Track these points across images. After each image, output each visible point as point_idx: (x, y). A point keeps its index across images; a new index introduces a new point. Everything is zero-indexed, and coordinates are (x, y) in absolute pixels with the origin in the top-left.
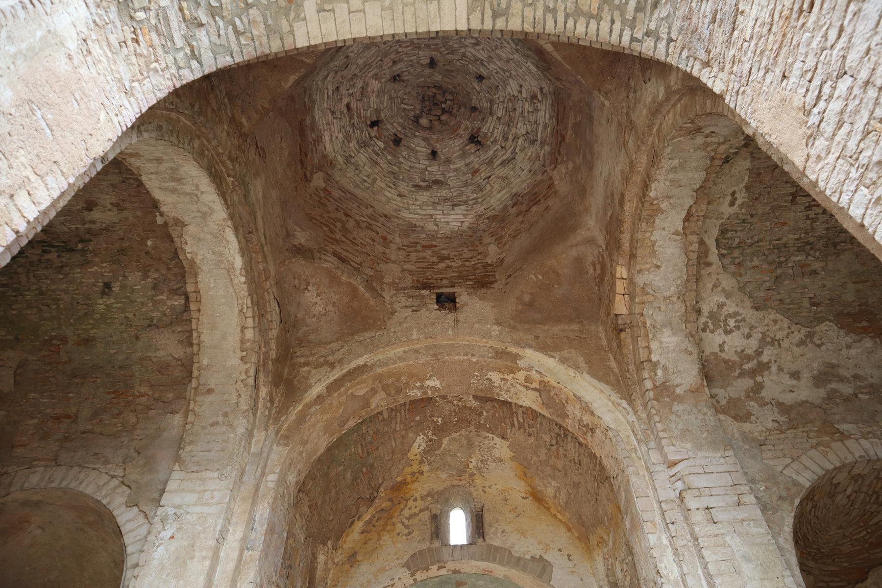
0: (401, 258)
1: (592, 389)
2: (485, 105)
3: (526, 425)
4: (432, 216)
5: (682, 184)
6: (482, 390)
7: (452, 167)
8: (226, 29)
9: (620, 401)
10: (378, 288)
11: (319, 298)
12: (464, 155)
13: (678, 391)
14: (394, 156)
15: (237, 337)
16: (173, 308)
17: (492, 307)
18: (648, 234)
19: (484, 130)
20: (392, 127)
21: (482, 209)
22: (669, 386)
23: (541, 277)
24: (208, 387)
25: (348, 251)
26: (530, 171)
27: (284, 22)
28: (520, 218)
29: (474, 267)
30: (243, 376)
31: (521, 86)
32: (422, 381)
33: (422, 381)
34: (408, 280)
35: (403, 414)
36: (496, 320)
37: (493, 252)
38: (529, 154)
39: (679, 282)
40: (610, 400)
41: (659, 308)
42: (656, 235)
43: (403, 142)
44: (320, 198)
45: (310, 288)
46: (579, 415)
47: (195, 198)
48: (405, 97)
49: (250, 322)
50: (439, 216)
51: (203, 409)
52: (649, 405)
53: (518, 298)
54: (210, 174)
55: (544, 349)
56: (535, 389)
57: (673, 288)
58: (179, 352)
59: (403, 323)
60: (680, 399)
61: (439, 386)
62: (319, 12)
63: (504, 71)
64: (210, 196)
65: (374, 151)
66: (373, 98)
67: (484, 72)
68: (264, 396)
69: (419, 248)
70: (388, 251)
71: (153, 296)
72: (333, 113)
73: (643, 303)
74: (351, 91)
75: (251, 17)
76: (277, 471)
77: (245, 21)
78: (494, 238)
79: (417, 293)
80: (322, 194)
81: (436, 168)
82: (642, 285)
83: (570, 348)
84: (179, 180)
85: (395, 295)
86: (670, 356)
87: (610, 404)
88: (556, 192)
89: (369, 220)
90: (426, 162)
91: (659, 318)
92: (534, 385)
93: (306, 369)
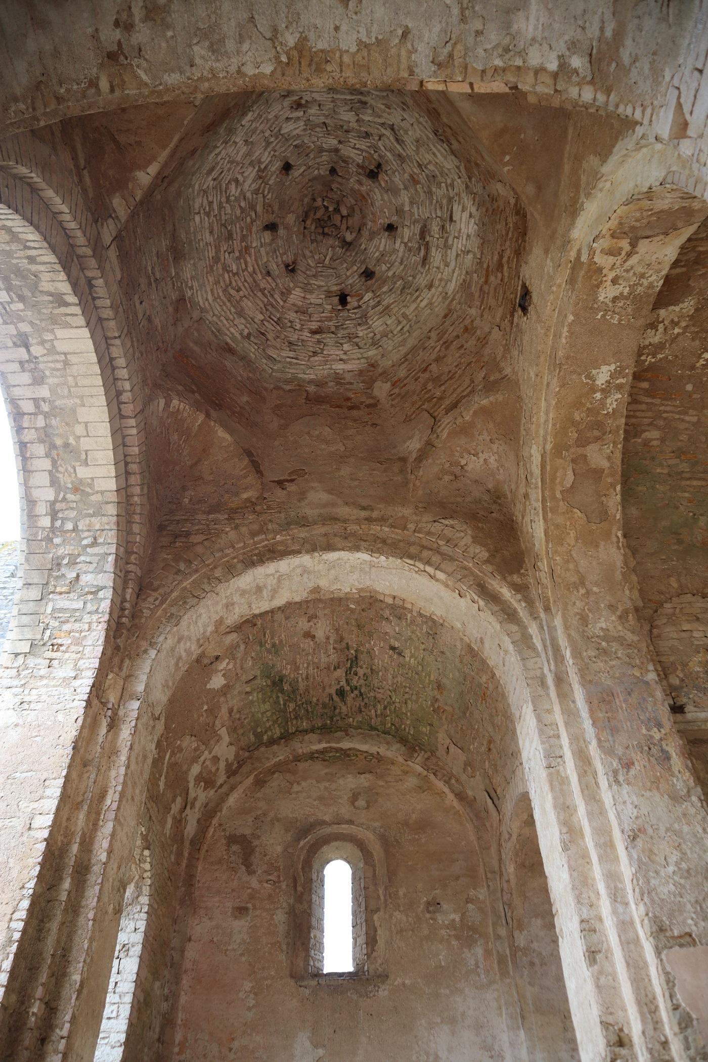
2: (324, 158)
4: (458, 255)
5: (246, 16)
7: (407, 208)
8: (88, 554)
11: (481, 455)
12: (392, 190)
14: (384, 282)
18: (346, 59)
20: (353, 279)
21: (459, 181)
23: (507, 158)
25: (455, 390)
27: (93, 498)
30: (476, 606)
32: (593, 390)
33: (593, 390)
41: (478, 33)
42: (348, 43)
44: (399, 394)
45: (463, 462)
48: (316, 257)
50: (460, 246)
54: (253, 564)
55: (574, 210)
61: (613, 367)
62: (87, 465)
65: (374, 307)
66: (313, 298)
67: (277, 165)
68: (509, 594)
70: (478, 332)
72: (315, 354)
73: (466, 67)
75: (85, 528)
77: (86, 534)
80: (396, 391)
81: (406, 230)
89: (441, 342)
90: (398, 241)
91: (493, 37)
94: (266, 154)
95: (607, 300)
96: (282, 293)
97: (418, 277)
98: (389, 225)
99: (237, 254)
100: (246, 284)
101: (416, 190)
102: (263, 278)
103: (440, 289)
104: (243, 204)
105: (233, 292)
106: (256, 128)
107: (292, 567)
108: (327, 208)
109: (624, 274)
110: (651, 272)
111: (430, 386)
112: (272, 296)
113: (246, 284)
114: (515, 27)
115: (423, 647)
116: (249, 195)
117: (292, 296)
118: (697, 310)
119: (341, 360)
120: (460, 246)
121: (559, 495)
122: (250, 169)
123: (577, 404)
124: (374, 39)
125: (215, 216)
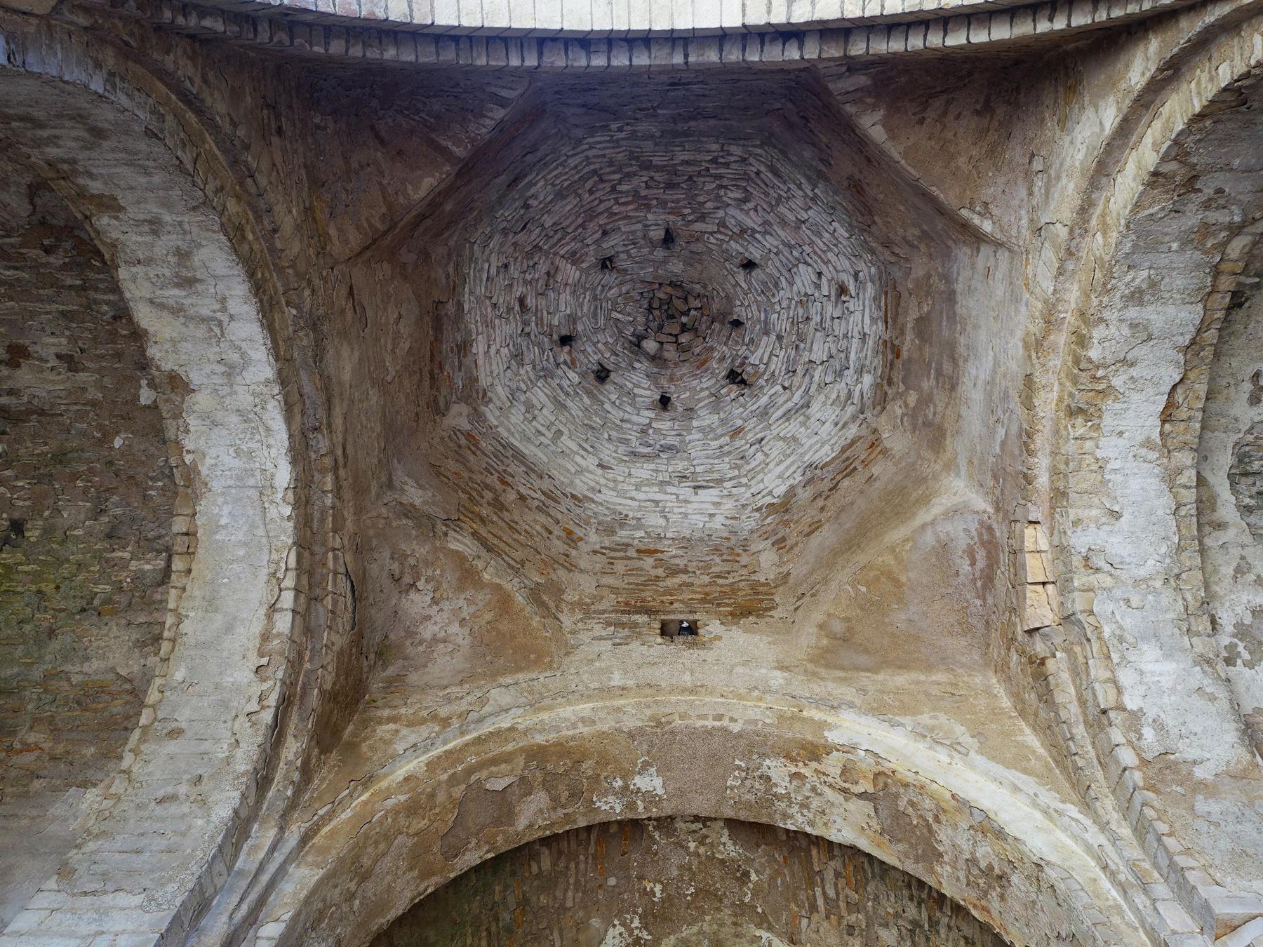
0: (598, 566)
1: (993, 786)
3: (842, 905)
4: (656, 503)
6: (749, 806)
9: (1061, 806)
10: (552, 605)
13: (1199, 773)
15: (257, 627)
16: (138, 577)
17: (769, 643)
18: (1089, 445)
19: (754, 359)
20: (593, 352)
21: (748, 495)
22: (1177, 763)
23: (864, 589)
24: (174, 725)
26: (836, 424)
28: (820, 502)
29: (734, 589)
30: (253, 706)
31: (820, 274)
34: (609, 601)
35: (582, 866)
36: (778, 661)
37: (767, 562)
38: (834, 396)
39: (1164, 549)
40: (1035, 805)
42: (1109, 447)
43: (613, 375)
44: (460, 446)
45: (420, 585)
46: (966, 847)
47: (217, 330)
49: (288, 599)
51: (151, 768)
52: (1138, 798)
53: (820, 627)
55: (878, 710)
56: (861, 796)
57: (1151, 562)
58: (130, 666)
59: (594, 661)
60: (1207, 789)
61: (660, 791)
63: (790, 247)
64: (247, 330)
67: (756, 254)
68: (291, 757)
69: (632, 553)
70: (574, 553)
71: (105, 550)
73: (1090, 590)
74: (528, 277)
76: (286, 917)
78: (770, 541)
79: (625, 619)
82: (1084, 551)
83: (935, 709)
84: (188, 283)
85: (582, 620)
86: (1166, 700)
87: (1038, 815)
88: (885, 452)
90: (651, 414)
91: (1130, 621)
92: (865, 786)
93: (392, 726)
94: (776, 243)
95: (764, 769)
96: (574, 253)
97: (610, 446)
98: (669, 399)
99: (643, 193)
100: (596, 202)
101: (722, 436)
102: (600, 226)
103: (603, 481)
104: (709, 205)
105: (589, 185)
106: (821, 237)
107: (243, 345)
108: (686, 313)
109: (808, 786)
110: (811, 816)
111: (488, 495)
112: (574, 239)
113: (596, 202)
114: (1145, 647)
115: (49, 589)
116: (721, 213)
117: (569, 266)
118: (722, 861)
119: (489, 346)
120: (669, 504)
121: (473, 778)
122: (760, 221)
123: (603, 761)
124: (1107, 477)
125: (708, 169)
